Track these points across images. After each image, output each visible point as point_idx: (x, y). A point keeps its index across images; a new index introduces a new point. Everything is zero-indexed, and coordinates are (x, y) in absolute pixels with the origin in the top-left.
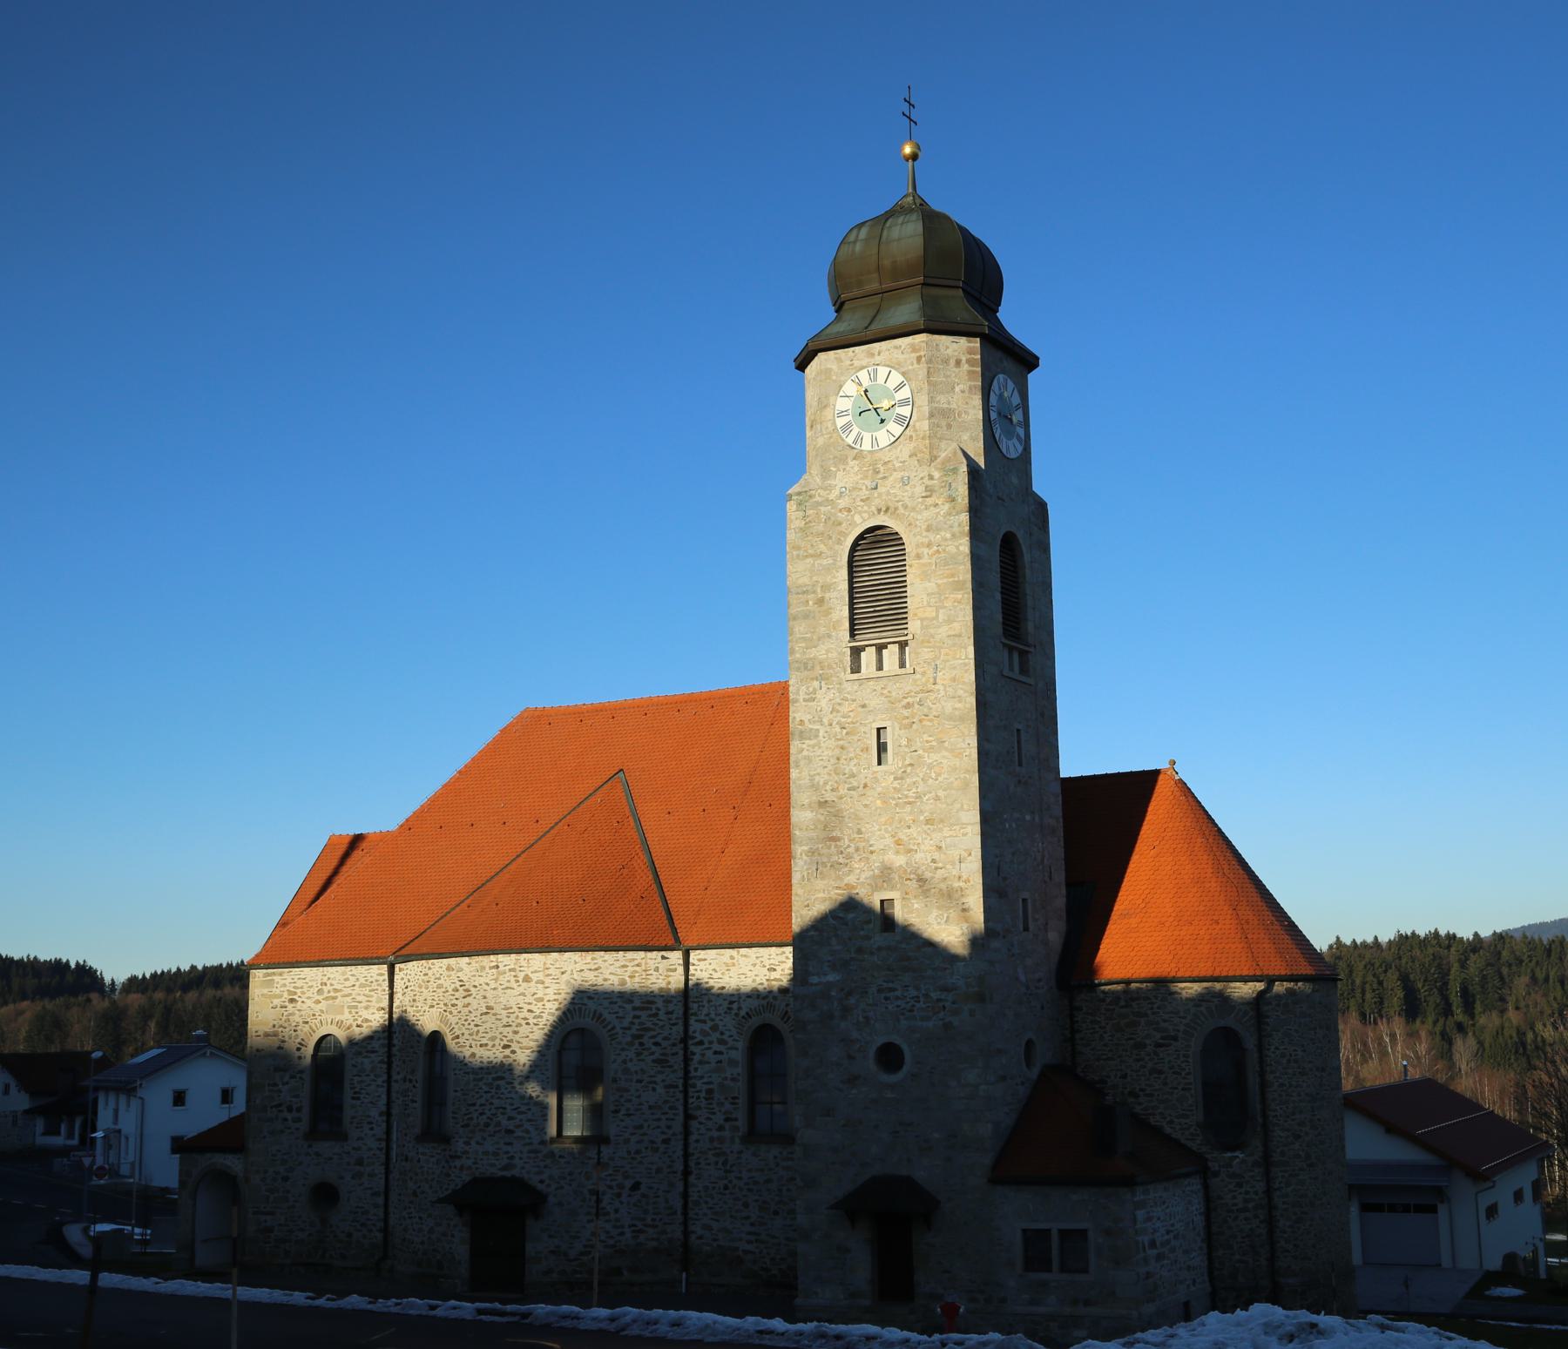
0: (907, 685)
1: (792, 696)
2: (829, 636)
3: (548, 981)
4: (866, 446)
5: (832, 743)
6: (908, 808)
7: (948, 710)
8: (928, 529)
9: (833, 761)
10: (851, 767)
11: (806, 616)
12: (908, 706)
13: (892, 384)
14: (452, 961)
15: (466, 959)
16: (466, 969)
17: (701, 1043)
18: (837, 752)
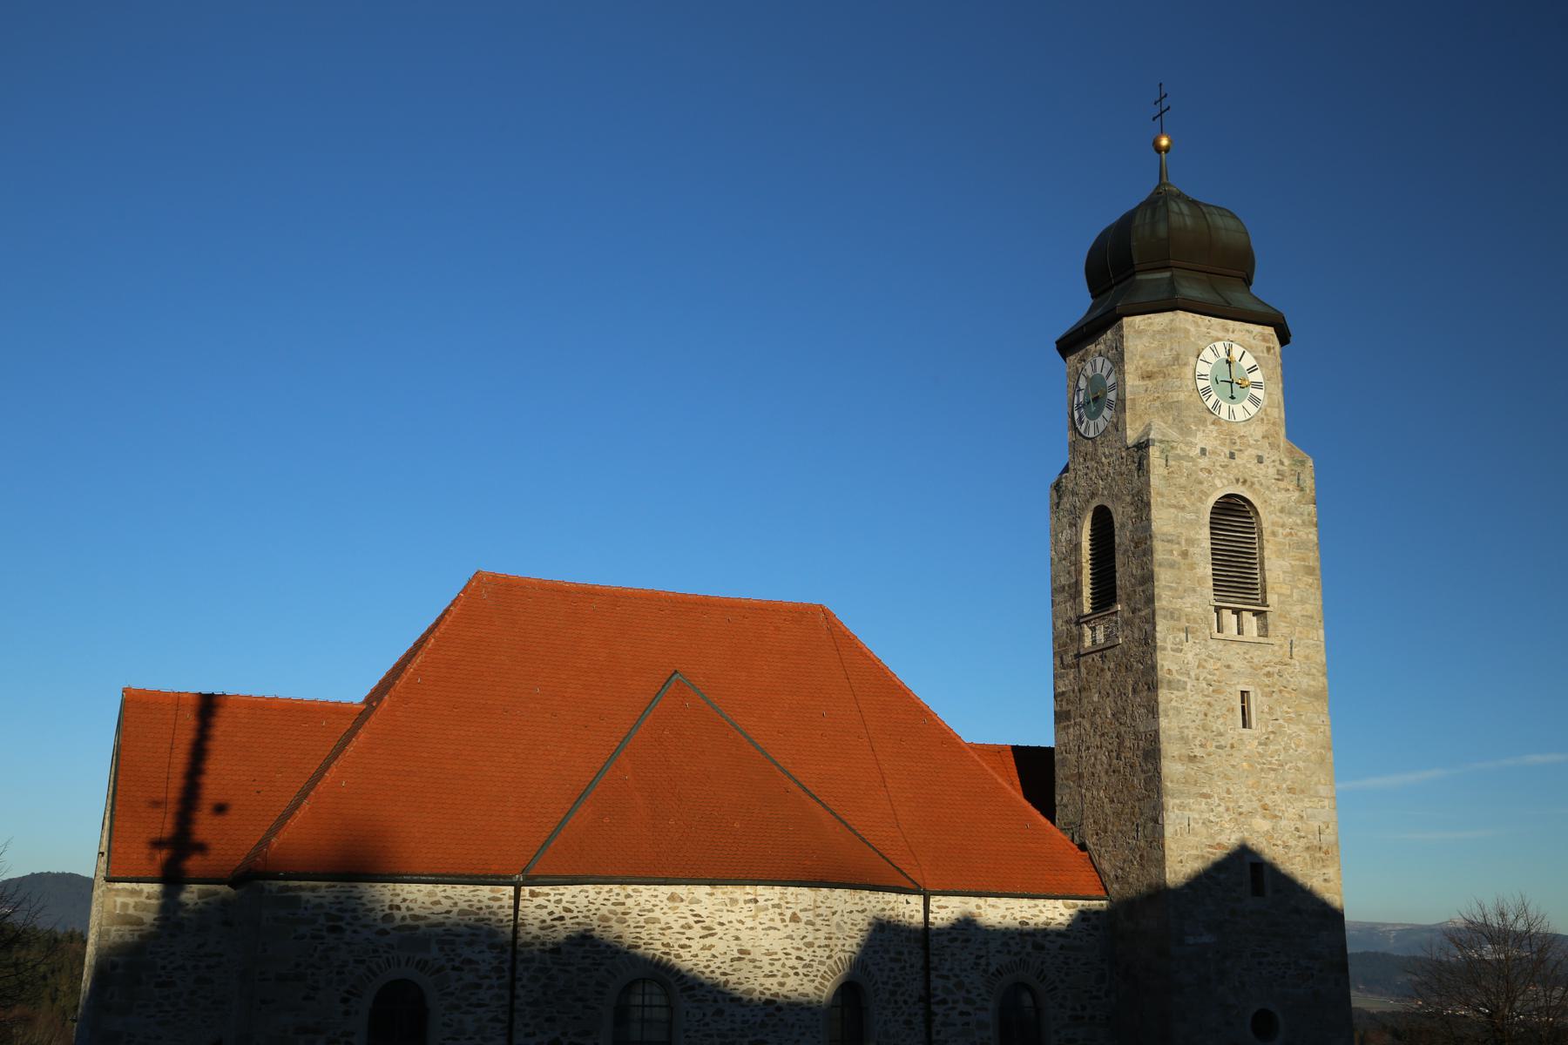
0: (1259, 656)
1: (1159, 643)
2: (1194, 590)
3: (818, 921)
4: (1224, 415)
5: (1199, 698)
6: (1272, 775)
7: (1304, 686)
8: (1282, 511)
9: (1201, 716)
10: (1218, 725)
11: (1172, 565)
12: (1268, 674)
13: (1213, 359)
14: (681, 890)
15: (707, 889)
16: (706, 901)
17: (944, 1002)
18: (1204, 708)
